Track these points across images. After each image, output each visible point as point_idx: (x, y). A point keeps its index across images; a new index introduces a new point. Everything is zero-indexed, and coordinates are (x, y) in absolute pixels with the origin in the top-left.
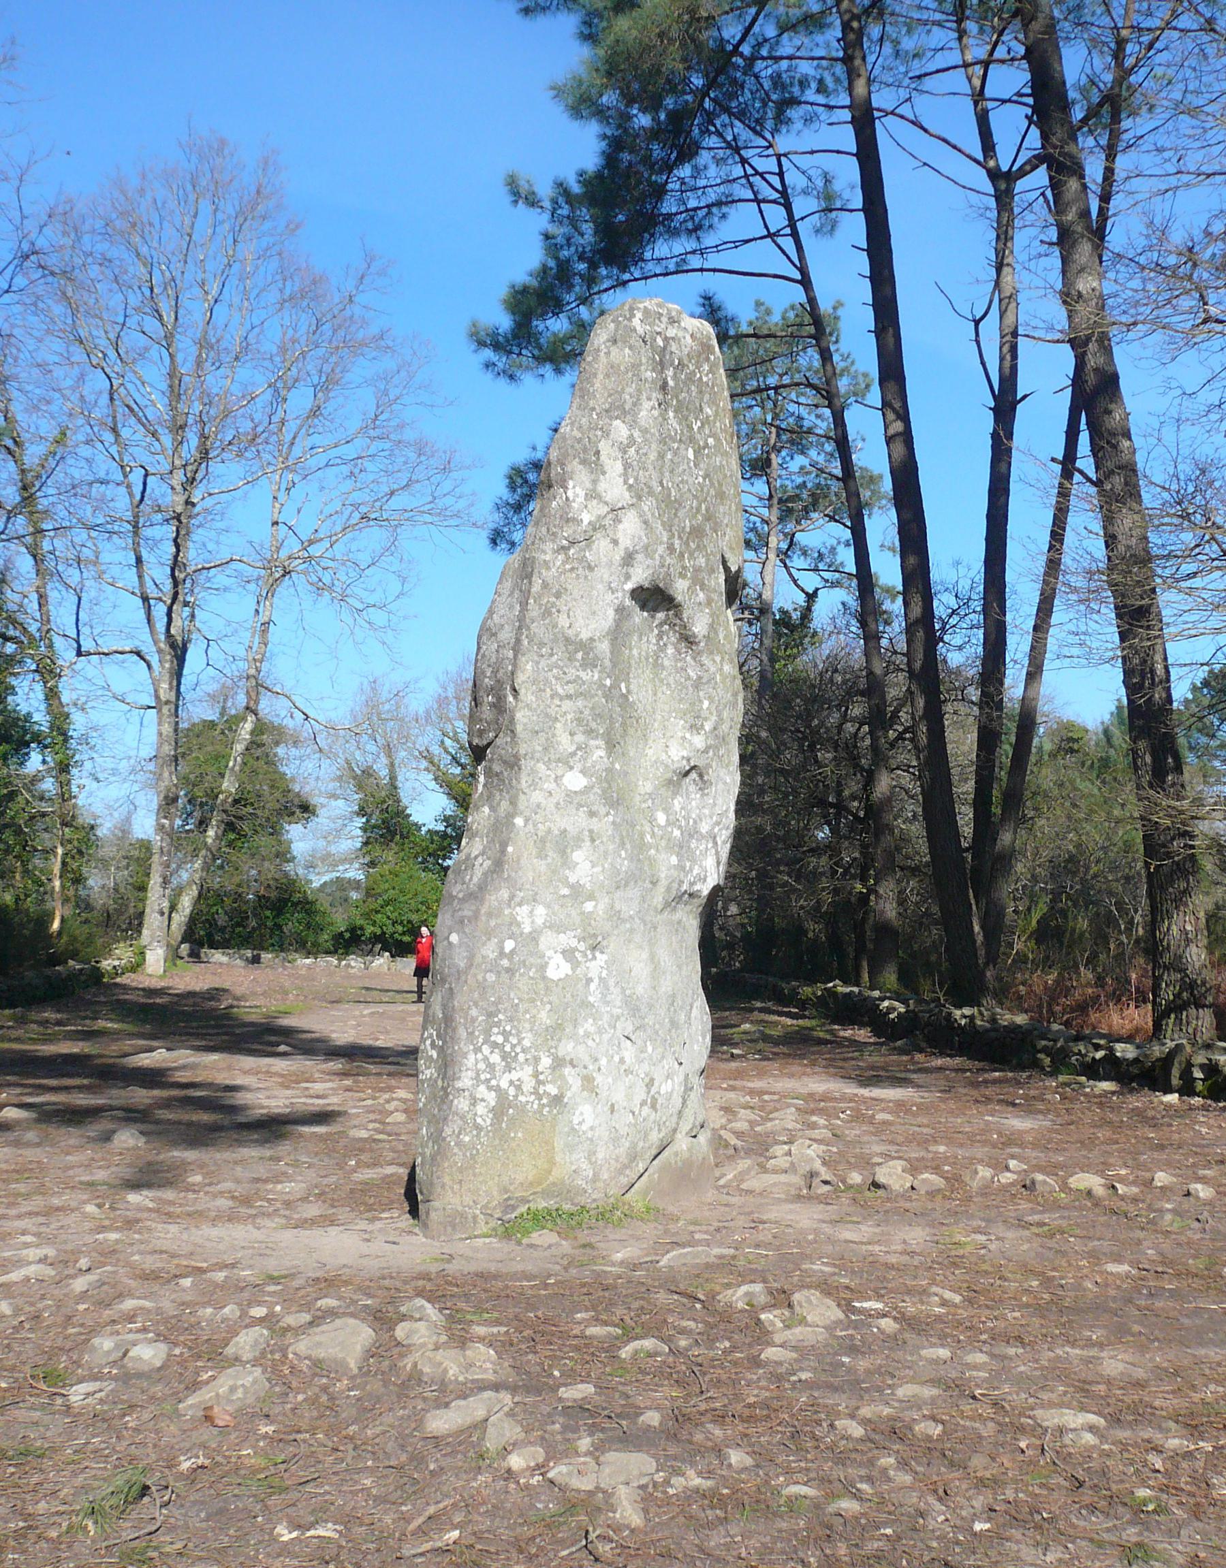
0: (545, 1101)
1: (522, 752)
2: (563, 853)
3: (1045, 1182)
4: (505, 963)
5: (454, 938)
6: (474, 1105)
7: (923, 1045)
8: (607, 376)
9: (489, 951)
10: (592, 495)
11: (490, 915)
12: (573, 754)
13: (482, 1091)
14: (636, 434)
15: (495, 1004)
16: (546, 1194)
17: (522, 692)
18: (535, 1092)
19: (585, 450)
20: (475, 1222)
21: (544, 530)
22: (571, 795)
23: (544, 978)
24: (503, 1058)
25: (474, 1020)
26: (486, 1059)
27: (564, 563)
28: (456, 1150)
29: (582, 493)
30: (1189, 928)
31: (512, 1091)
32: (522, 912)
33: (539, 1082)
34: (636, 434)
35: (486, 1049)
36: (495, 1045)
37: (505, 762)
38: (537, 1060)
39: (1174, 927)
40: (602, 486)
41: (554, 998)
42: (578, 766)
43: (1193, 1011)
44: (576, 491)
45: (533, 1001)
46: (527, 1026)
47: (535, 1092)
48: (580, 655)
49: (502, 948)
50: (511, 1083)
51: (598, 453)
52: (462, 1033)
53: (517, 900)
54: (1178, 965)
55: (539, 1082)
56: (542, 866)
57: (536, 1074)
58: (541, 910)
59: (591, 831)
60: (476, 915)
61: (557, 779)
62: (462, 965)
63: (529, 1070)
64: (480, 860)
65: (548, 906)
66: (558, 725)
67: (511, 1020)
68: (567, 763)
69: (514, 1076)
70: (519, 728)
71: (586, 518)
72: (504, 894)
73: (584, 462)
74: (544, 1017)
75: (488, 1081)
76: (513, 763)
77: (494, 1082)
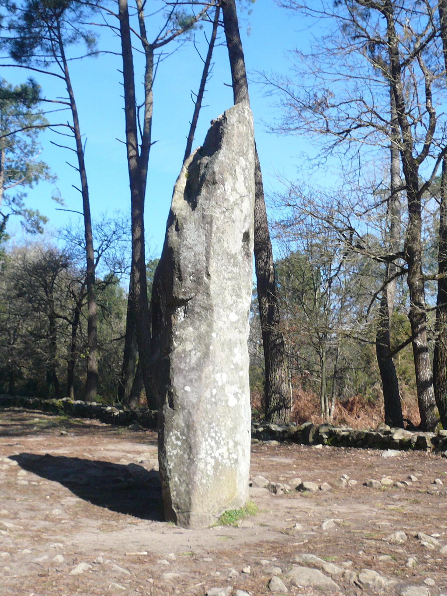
0: (232, 462)
1: (214, 303)
2: (230, 349)
3: (376, 483)
4: (213, 400)
5: (188, 388)
6: (206, 465)
7: (141, 427)
8: (238, 137)
9: (207, 394)
10: (234, 189)
11: (206, 378)
12: (232, 305)
13: (209, 459)
14: (248, 164)
15: (211, 419)
16: (232, 504)
17: (212, 276)
18: (229, 458)
19: (231, 169)
20: (210, 519)
21: (214, 203)
22: (232, 323)
23: (228, 406)
24: (216, 443)
25: (204, 426)
26: (209, 444)
27: (224, 219)
28: (200, 487)
29: (230, 188)
30: (283, 376)
31: (220, 458)
32: (218, 376)
33: (230, 453)
34: (248, 164)
35: (209, 439)
36: (212, 438)
37: (202, 307)
38: (228, 443)
39: (277, 376)
40: (237, 186)
41: (232, 415)
42: (234, 311)
43: (284, 410)
44: (228, 186)
45: (224, 416)
46: (223, 428)
47: (229, 458)
48: (232, 261)
49: (212, 393)
50: (220, 454)
51: (235, 171)
52: (199, 433)
53: (216, 371)
54: (278, 391)
55: (230, 453)
56: (223, 355)
57: (228, 450)
58: (224, 375)
59: (240, 340)
60: (200, 378)
61: (227, 316)
62: (195, 401)
63: (225, 448)
64: (193, 352)
65: (227, 373)
66: (226, 292)
67: (217, 426)
68: (230, 309)
69: (220, 451)
70: (212, 292)
71: (232, 199)
72: (211, 368)
73: (231, 174)
74: (230, 424)
75: (211, 454)
76: (209, 308)
77: (213, 455)
